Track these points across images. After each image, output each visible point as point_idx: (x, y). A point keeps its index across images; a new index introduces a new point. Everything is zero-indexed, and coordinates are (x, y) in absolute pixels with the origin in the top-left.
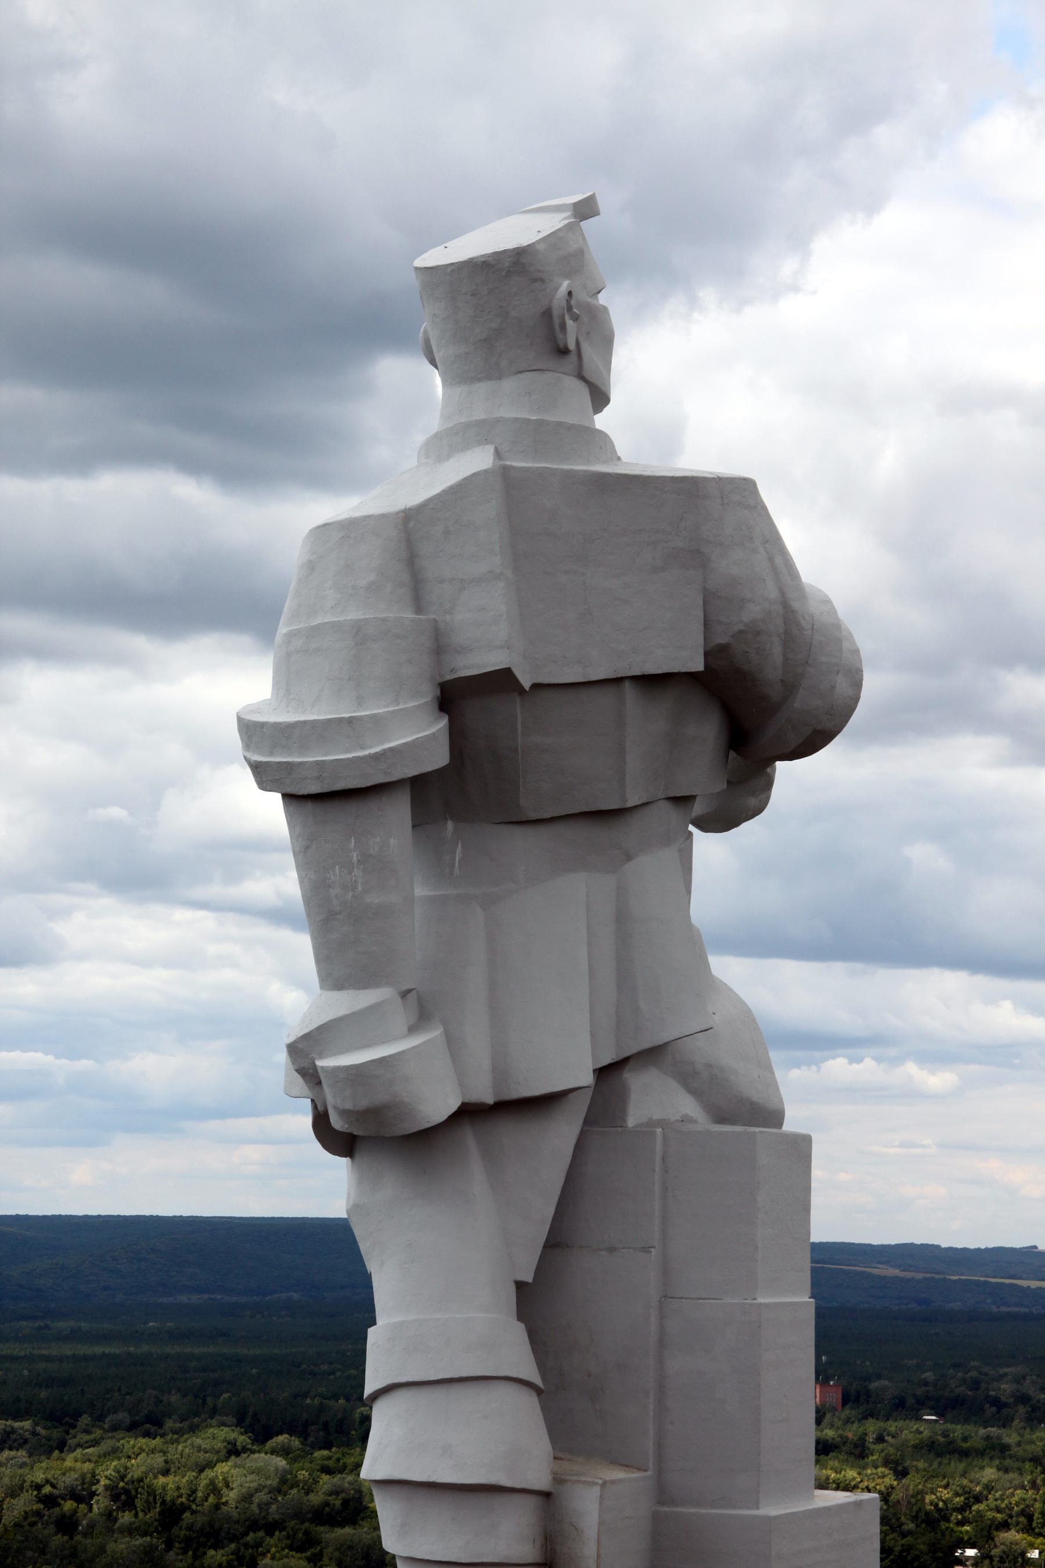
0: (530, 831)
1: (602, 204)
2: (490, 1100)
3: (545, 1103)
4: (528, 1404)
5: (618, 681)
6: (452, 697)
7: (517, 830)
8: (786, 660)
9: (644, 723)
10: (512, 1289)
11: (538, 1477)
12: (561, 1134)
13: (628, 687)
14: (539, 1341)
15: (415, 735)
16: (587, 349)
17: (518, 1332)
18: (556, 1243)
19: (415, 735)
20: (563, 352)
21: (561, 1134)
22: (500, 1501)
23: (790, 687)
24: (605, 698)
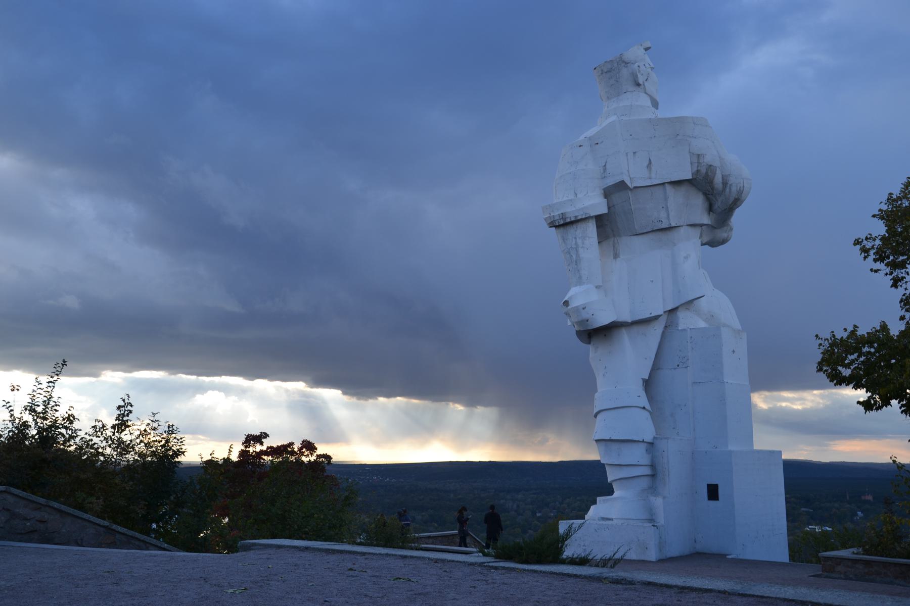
0: (640, 237)
1: (713, 503)
2: (630, 321)
3: (656, 318)
4: (646, 414)
5: (663, 184)
6: (608, 193)
7: (635, 237)
8: (707, 173)
9: (675, 197)
10: (641, 382)
11: (649, 438)
12: (656, 330)
13: (668, 187)
14: (650, 398)
15: (597, 204)
16: (646, 84)
17: (643, 394)
18: (656, 367)
19: (597, 204)
20: (638, 85)
21: (656, 330)
22: (635, 445)
23: (725, 183)
24: (658, 192)
